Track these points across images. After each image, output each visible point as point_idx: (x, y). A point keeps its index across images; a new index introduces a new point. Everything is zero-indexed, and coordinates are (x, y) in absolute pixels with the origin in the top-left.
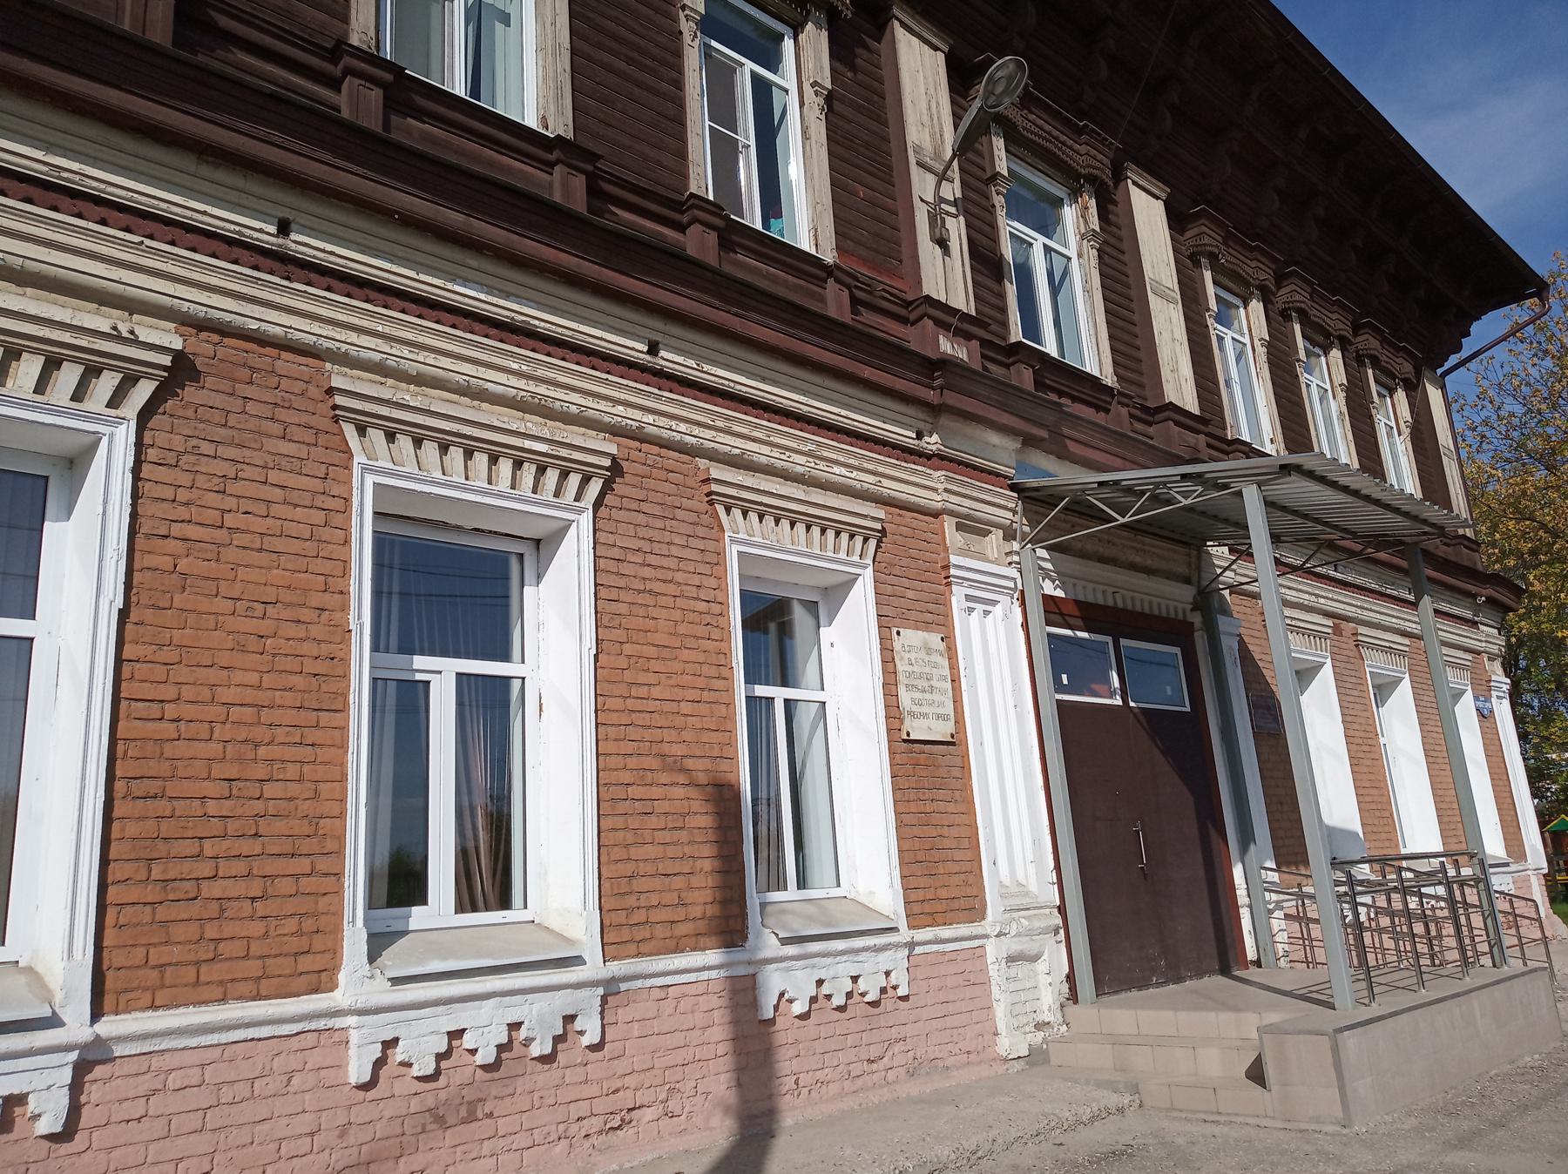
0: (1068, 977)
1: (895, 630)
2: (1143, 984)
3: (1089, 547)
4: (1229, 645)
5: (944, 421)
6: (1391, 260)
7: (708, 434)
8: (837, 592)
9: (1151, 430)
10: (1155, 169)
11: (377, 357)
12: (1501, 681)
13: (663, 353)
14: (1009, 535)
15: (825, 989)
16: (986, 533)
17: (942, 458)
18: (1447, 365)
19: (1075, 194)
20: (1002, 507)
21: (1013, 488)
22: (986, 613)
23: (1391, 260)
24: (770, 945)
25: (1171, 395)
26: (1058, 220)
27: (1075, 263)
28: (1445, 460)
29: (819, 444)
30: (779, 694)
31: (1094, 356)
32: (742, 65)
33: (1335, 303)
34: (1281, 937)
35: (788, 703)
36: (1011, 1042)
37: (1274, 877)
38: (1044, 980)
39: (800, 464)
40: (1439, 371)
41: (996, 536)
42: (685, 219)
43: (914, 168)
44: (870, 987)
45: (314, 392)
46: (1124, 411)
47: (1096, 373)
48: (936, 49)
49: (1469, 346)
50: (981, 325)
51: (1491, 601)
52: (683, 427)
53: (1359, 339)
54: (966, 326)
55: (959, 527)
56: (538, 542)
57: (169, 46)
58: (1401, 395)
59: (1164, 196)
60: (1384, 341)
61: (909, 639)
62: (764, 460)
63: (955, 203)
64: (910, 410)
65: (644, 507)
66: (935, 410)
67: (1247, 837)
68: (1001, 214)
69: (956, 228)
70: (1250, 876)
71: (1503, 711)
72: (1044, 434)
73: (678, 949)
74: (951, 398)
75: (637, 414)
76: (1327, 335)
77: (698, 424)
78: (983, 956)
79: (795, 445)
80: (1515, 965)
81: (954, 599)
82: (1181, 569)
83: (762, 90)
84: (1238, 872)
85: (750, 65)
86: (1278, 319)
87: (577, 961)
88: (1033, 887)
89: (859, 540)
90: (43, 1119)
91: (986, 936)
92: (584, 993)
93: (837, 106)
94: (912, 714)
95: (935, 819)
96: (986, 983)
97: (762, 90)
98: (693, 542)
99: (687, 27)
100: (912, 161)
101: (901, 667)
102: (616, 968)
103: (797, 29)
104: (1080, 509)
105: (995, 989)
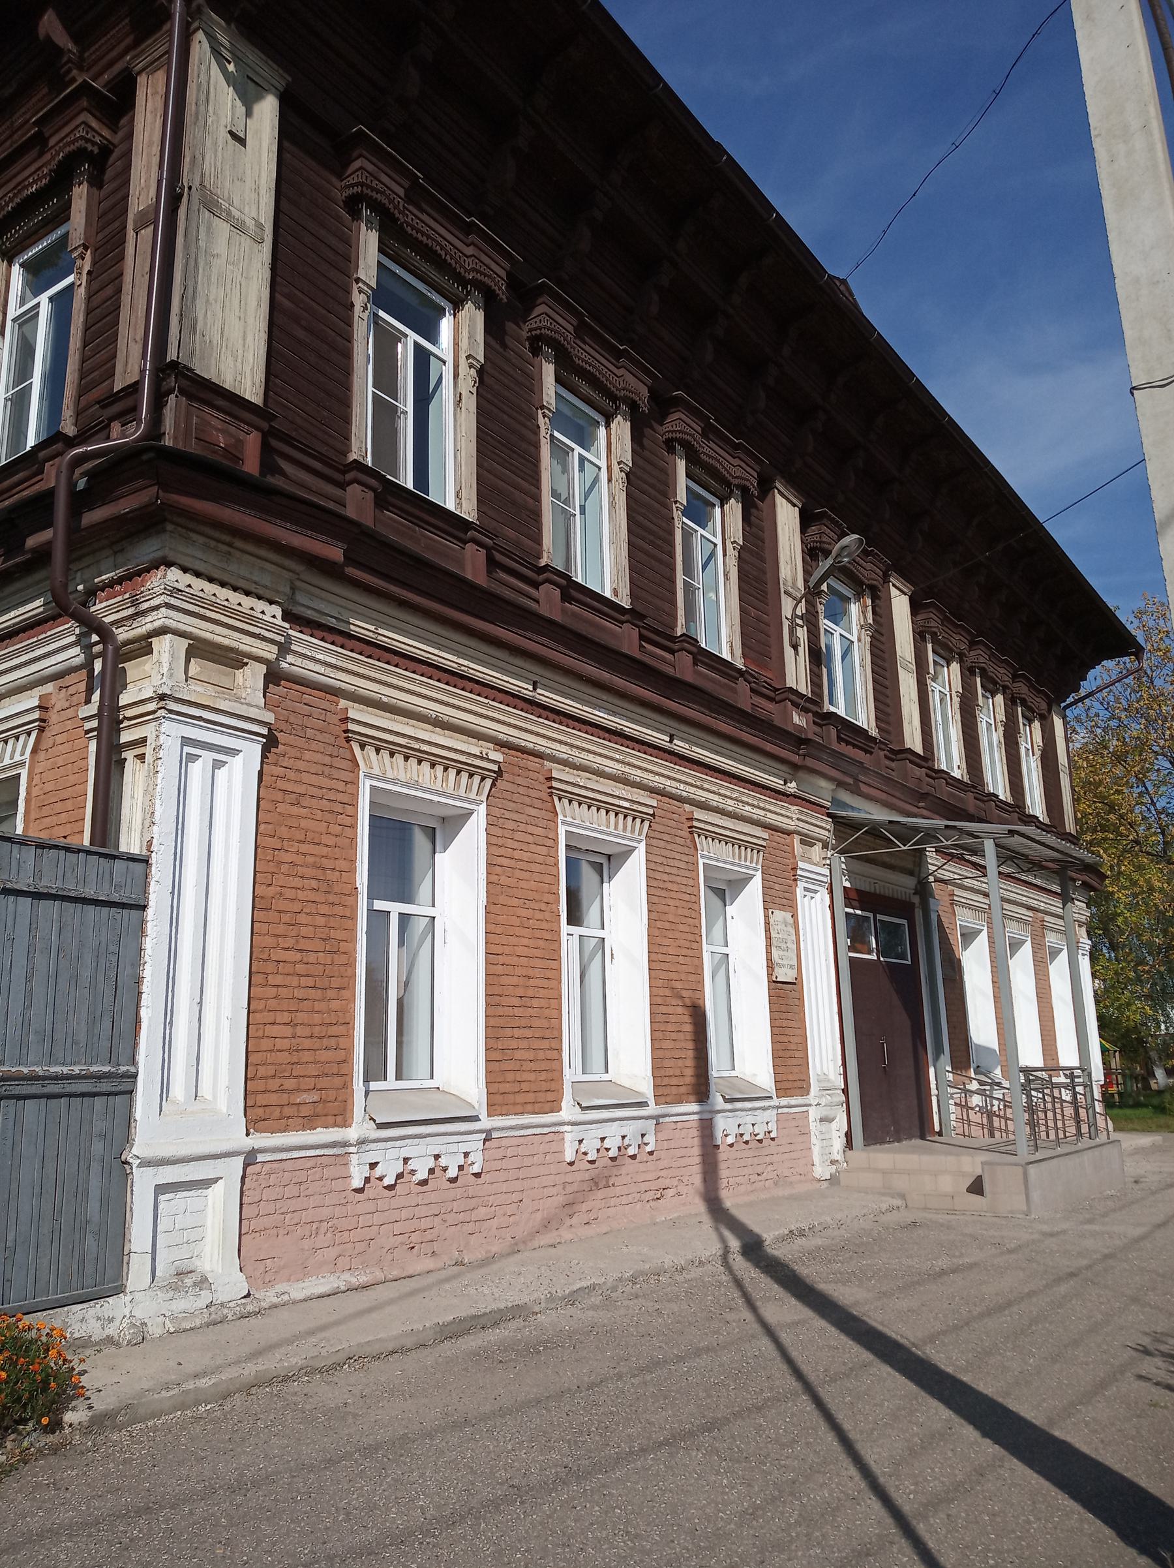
0: (846, 1134)
2: (882, 1142)
3: (887, 859)
4: (934, 917)
5: (801, 774)
6: (1028, 612)
7: (692, 790)
8: (453, 822)
9: (893, 765)
10: (906, 575)
11: (565, 756)
12: (1086, 943)
13: (675, 741)
14: (825, 846)
15: (378, 1172)
16: (812, 845)
17: (795, 796)
18: (1070, 700)
19: (859, 596)
20: (823, 828)
21: (829, 815)
22: (217, 765)
23: (1028, 612)
24: (718, 1102)
25: (908, 744)
26: (845, 612)
27: (856, 644)
28: (1061, 774)
29: (741, 792)
30: (395, 908)
31: (865, 719)
32: (573, 450)
33: (1039, 692)
34: (953, 1117)
35: (404, 918)
36: (822, 1171)
37: (950, 1077)
38: (835, 1134)
39: (730, 805)
40: (1063, 705)
41: (818, 847)
42: (676, 647)
43: (783, 595)
44: (760, 1130)
45: (542, 779)
46: (882, 753)
47: (865, 727)
48: (794, 505)
49: (1086, 687)
50: (811, 704)
51: (1084, 884)
52: (682, 786)
53: (1015, 685)
54: (808, 705)
55: (802, 842)
56: (609, 856)
57: (257, 475)
58: (1037, 725)
59: (407, 186)
60: (1031, 686)
61: (779, 916)
62: (715, 804)
63: (801, 618)
64: (784, 768)
66: (795, 767)
67: (939, 1051)
68: (821, 616)
69: (802, 633)
70: (938, 1074)
71: (1085, 964)
72: (851, 781)
73: (680, 1102)
74: (810, 762)
75: (662, 780)
76: (995, 683)
77: (688, 784)
78: (807, 1117)
80: (1103, 1137)
81: (798, 890)
82: (910, 866)
83: (422, 358)
84: (932, 1071)
85: (413, 336)
86: (968, 673)
87: (476, 1119)
88: (832, 1076)
89: (477, 779)
90: (475, 1166)
91: (810, 1105)
93: (486, 378)
94: (778, 965)
95: (788, 1031)
96: (808, 1134)
97: (422, 358)
99: (359, 300)
100: (782, 590)
101: (773, 935)
102: (260, 1140)
103: (457, 305)
104: (874, 832)
105: (813, 1139)
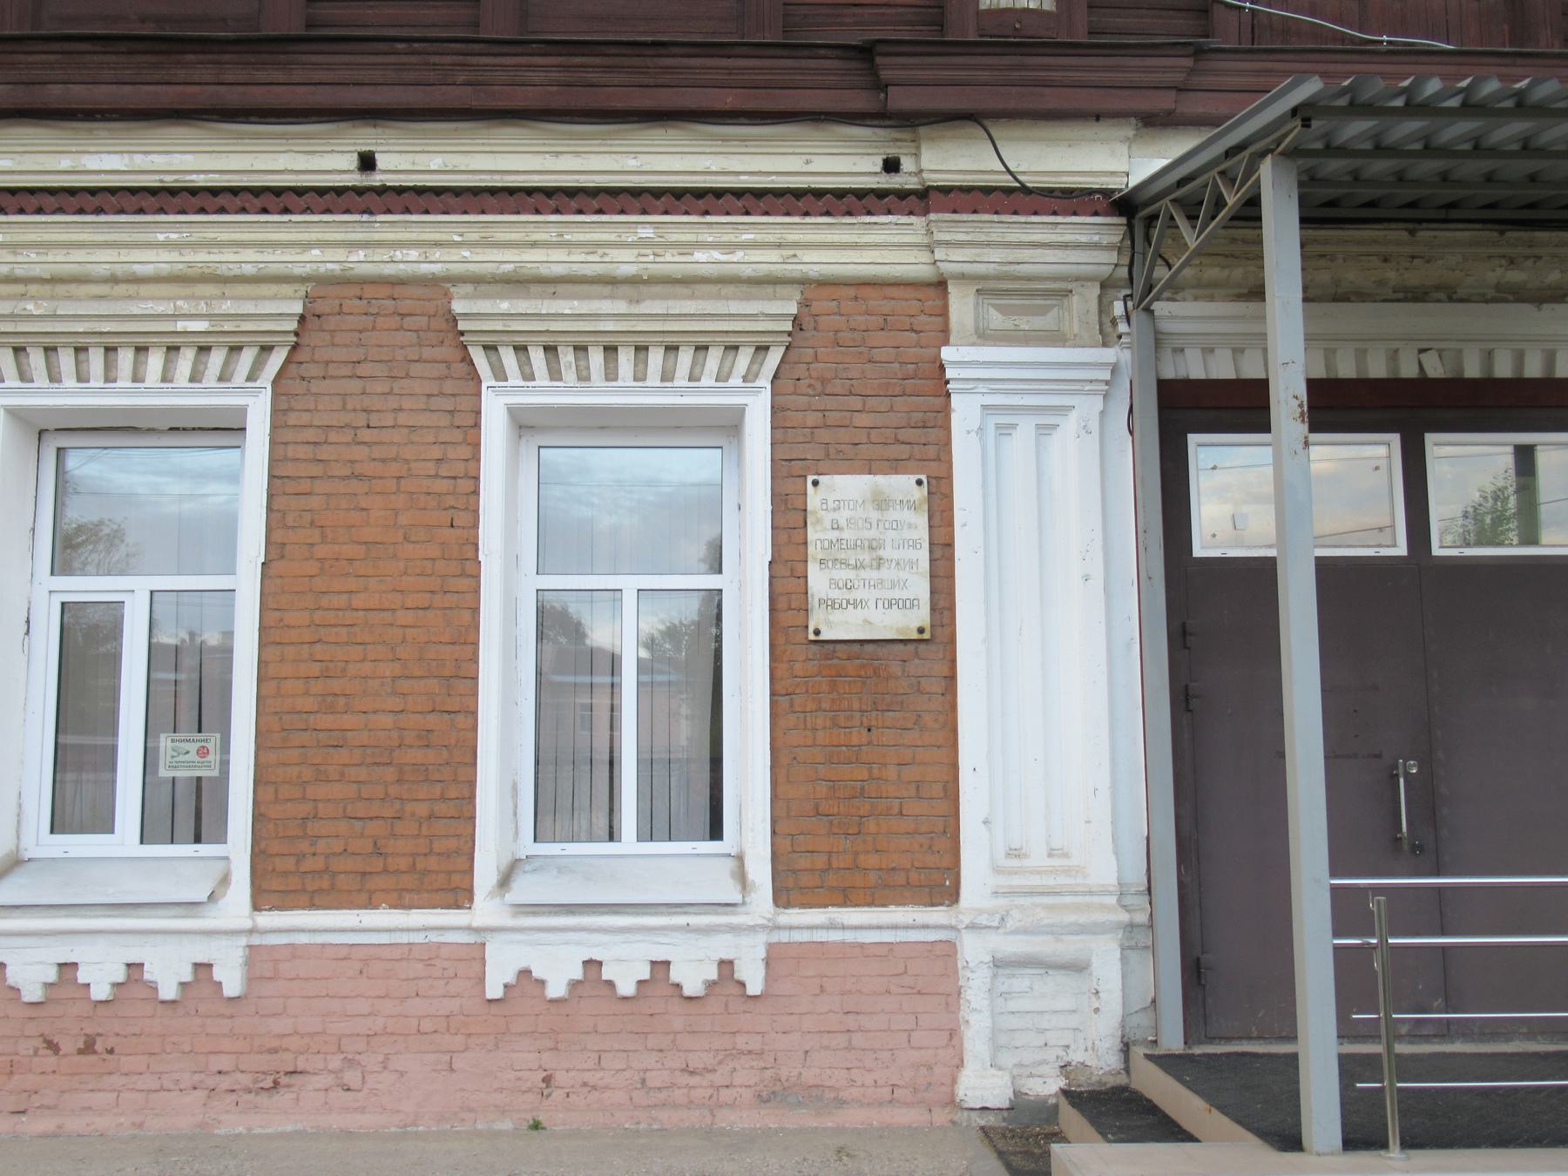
1: (810, 479)
22: (1045, 430)
65: (363, 370)
75: (340, 254)
79: (613, 237)
92: (224, 942)
98: (437, 403)
